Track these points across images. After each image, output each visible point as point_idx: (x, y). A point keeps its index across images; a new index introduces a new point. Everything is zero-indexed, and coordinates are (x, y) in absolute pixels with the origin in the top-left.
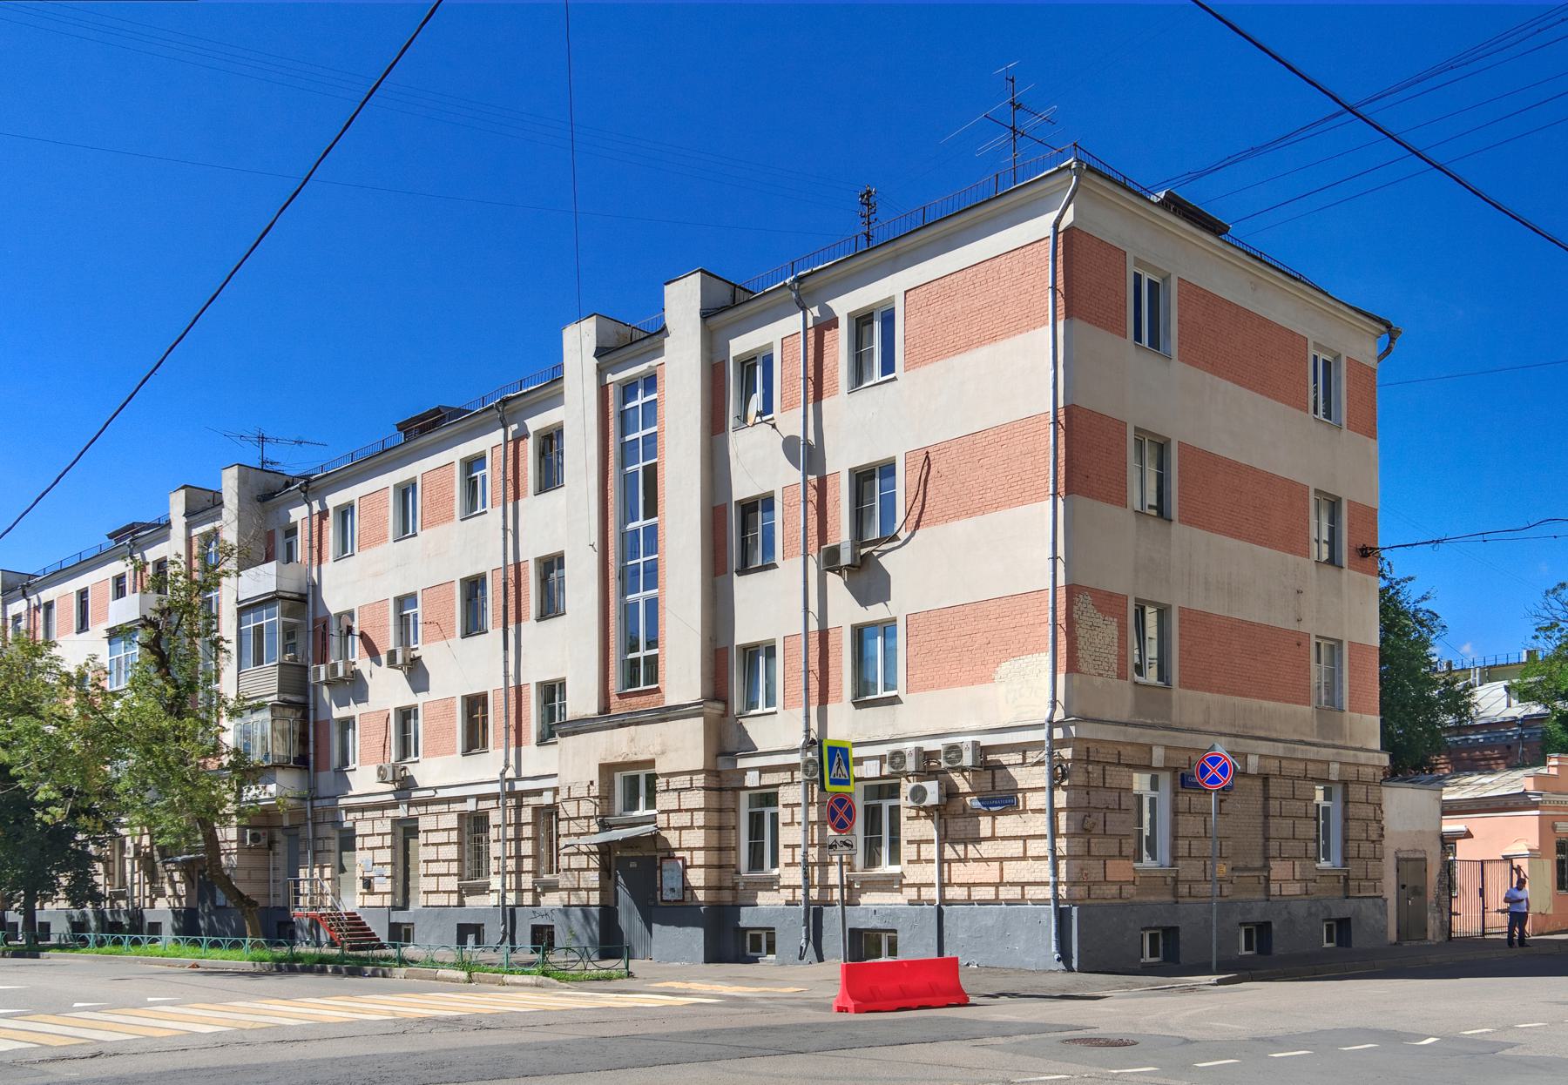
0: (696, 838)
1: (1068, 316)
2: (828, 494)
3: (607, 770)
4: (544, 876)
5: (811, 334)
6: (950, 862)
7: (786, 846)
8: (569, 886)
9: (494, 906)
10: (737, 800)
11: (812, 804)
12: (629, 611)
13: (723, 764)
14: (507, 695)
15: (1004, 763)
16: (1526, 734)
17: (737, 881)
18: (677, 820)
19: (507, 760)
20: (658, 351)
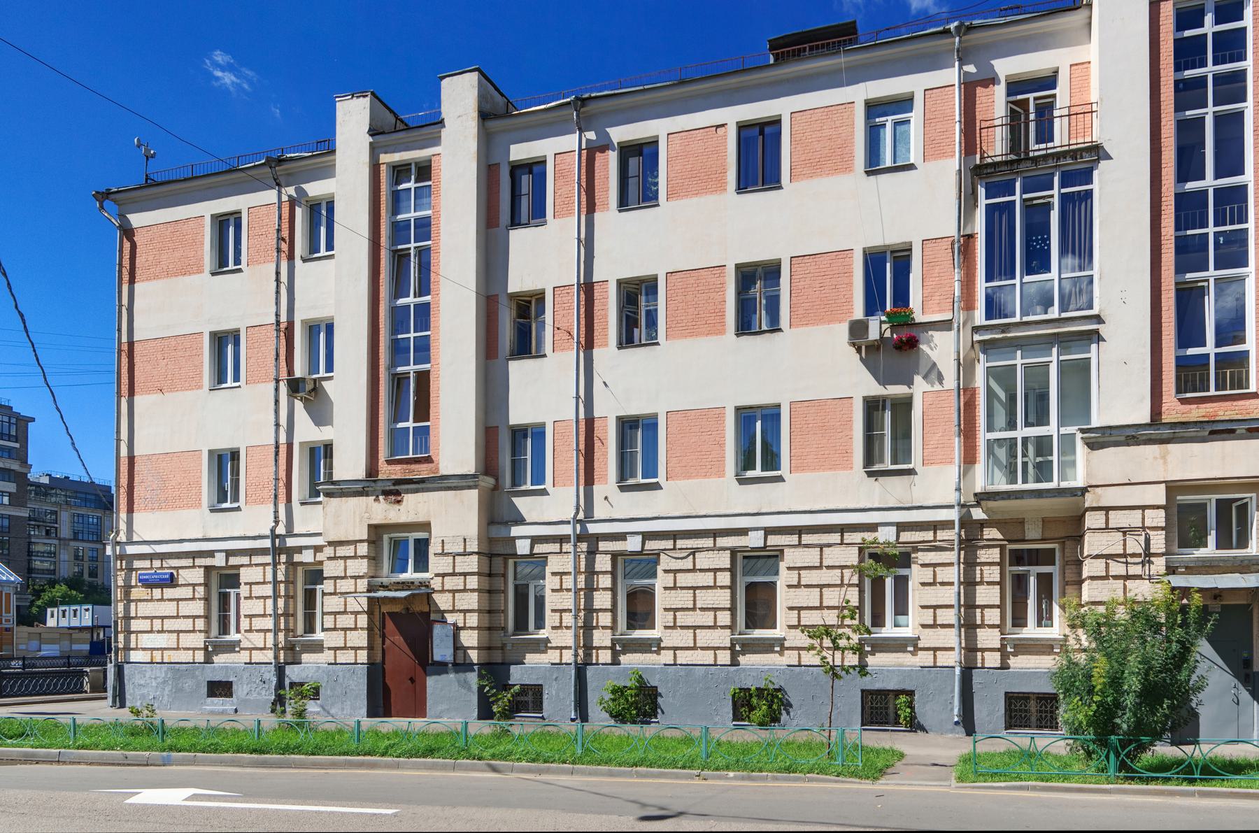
0: (471, 601)
7: (246, 616)
9: (246, 663)
13: (497, 532)
18: (451, 583)
19: (276, 517)
20: (436, 141)
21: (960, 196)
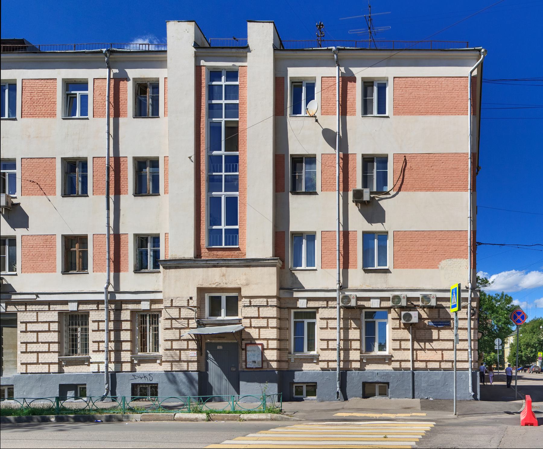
1: (473, 115)
2: (349, 163)
3: (201, 291)
4: (139, 353)
5: (112, 82)
6: (417, 350)
8: (171, 360)
10: (289, 314)
11: (110, 321)
12: (215, 202)
14: (109, 239)
15: (444, 306)
17: (290, 358)
19: (109, 279)
20: (244, 58)
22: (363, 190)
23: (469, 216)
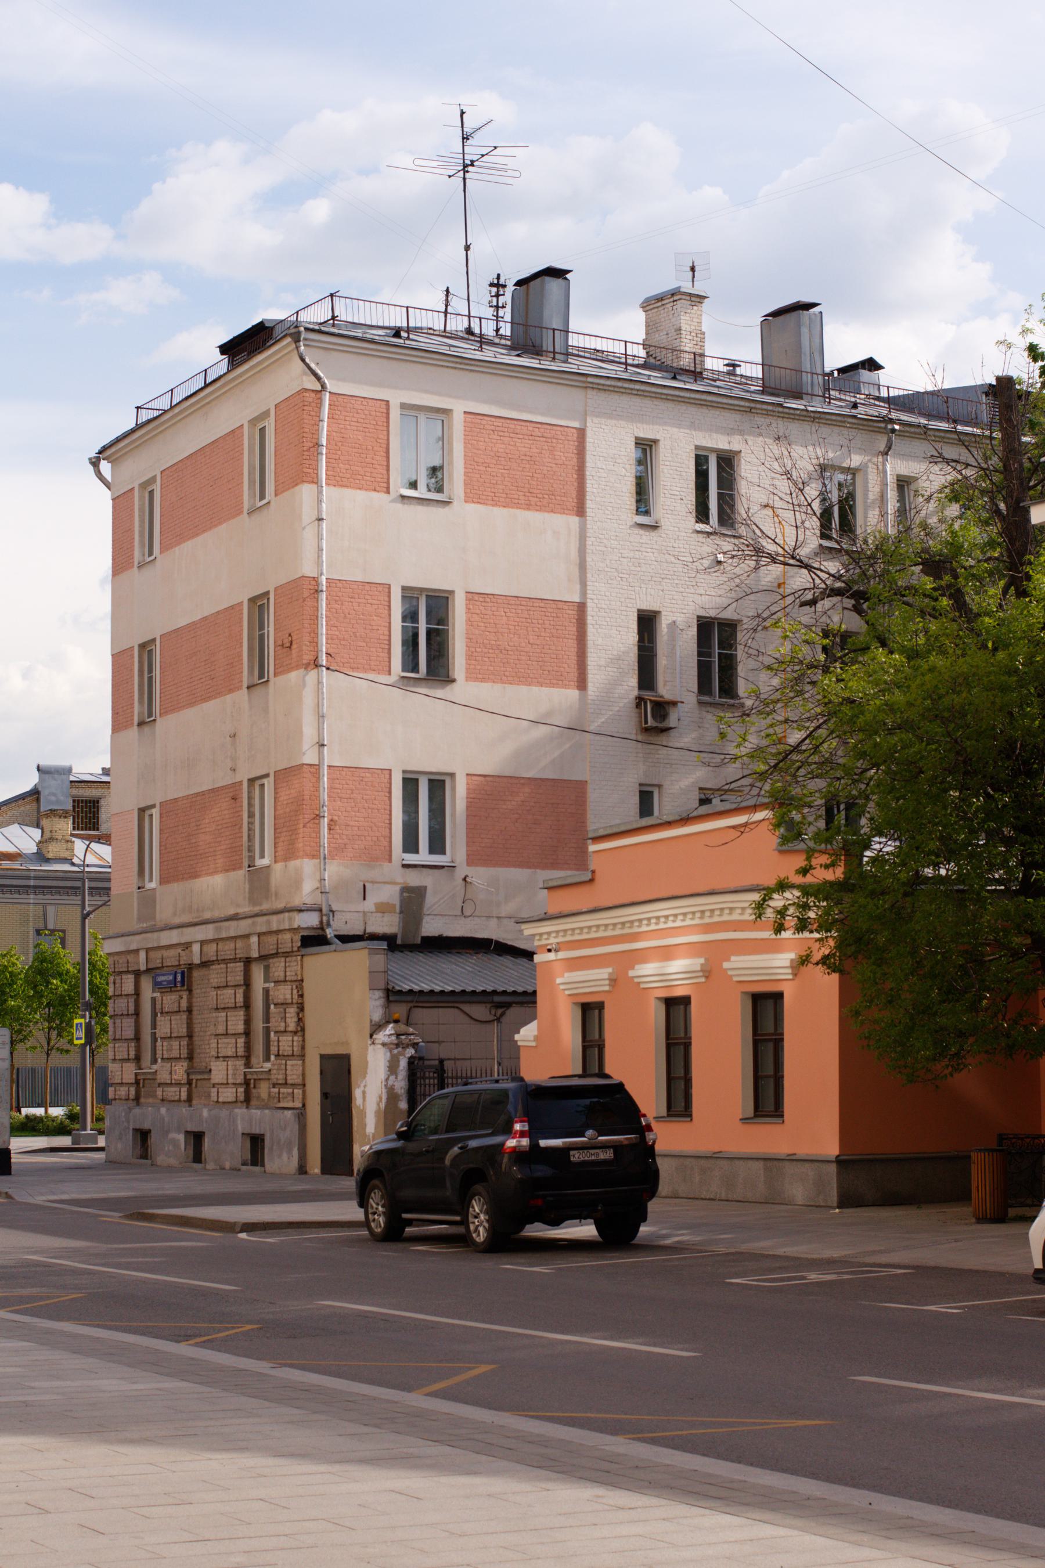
16: (835, 960)
21: (161, 432)
22: (351, 1174)
23: (345, 313)
